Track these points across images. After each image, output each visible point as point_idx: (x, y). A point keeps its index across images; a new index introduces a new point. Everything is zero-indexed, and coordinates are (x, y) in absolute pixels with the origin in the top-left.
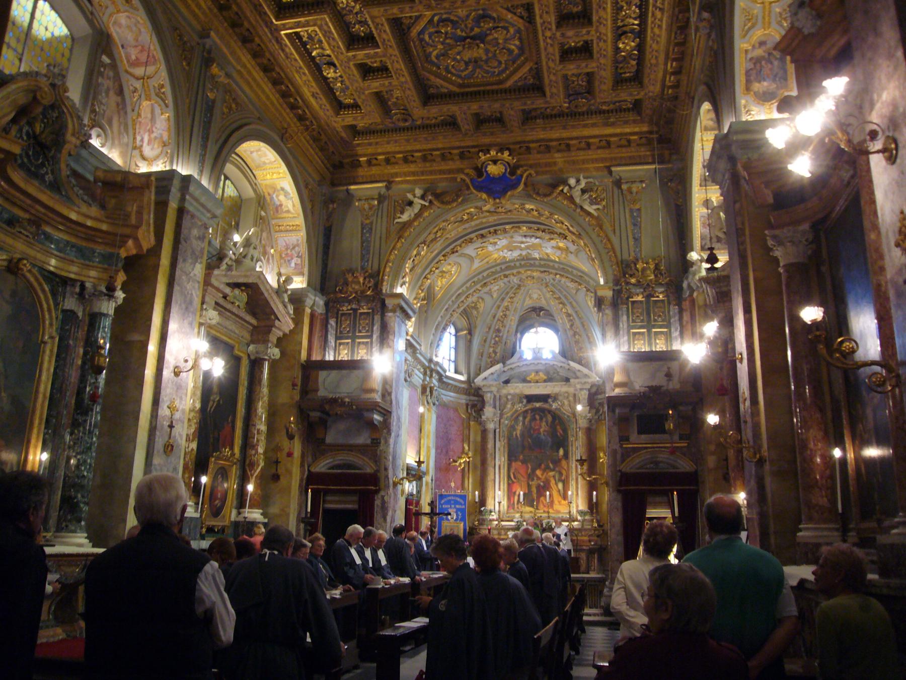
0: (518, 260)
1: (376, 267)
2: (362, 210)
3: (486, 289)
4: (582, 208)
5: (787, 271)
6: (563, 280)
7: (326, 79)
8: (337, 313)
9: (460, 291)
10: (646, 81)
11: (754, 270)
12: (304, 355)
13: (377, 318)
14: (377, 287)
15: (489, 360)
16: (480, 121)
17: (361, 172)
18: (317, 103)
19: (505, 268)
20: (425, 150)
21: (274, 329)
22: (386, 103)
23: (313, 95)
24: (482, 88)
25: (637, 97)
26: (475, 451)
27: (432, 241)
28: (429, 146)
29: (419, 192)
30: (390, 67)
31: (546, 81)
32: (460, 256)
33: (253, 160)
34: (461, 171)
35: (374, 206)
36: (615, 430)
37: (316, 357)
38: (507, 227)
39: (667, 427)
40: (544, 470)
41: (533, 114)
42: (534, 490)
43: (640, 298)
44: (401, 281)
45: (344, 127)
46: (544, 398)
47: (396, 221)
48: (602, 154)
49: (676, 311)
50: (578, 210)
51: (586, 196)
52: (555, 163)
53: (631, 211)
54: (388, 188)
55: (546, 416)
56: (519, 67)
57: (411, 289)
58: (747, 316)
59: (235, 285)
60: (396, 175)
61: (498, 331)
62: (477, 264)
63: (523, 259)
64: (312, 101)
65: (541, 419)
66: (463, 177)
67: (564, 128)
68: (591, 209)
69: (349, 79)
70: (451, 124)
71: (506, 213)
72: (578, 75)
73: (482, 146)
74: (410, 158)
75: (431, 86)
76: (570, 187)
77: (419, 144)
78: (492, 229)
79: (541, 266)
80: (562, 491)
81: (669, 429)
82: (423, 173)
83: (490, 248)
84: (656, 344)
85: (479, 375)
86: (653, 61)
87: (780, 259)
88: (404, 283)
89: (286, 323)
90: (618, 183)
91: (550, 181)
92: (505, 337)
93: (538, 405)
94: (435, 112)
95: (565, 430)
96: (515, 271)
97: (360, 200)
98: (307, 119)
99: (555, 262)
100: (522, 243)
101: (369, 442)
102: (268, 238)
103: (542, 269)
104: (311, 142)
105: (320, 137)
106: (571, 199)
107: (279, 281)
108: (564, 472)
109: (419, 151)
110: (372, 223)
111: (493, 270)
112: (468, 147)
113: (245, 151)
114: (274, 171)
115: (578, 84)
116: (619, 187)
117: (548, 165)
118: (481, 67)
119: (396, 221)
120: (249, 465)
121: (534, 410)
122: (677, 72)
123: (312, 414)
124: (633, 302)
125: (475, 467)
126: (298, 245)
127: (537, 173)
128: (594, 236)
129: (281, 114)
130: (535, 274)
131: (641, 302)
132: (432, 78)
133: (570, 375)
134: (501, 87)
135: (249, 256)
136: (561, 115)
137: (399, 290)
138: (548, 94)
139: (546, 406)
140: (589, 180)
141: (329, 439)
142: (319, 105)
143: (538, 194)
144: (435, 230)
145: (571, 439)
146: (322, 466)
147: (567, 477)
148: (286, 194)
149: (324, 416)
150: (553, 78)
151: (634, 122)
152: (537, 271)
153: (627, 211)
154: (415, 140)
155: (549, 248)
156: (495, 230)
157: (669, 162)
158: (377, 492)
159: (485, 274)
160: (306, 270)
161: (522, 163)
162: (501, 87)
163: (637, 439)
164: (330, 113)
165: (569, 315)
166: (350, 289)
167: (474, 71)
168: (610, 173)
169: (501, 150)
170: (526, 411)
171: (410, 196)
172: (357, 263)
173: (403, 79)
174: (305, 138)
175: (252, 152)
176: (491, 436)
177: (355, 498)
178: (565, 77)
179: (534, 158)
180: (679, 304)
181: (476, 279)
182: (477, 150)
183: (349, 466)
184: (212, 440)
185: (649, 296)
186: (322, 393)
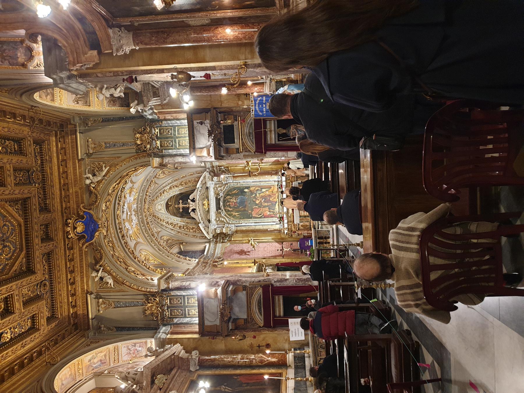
0: (138, 217)
1: (142, 297)
2: (106, 309)
3: (156, 235)
4: (104, 176)
5: (138, 44)
6: (149, 190)
7: (11, 339)
8: (170, 318)
9: (157, 249)
10: (20, 136)
11: (139, 66)
12: (196, 336)
13: (173, 293)
14: (153, 295)
15: (197, 232)
16: (47, 238)
17: (80, 312)
18: (29, 344)
19: (144, 225)
20: (66, 272)
21: (180, 356)
22: (32, 298)
23: (24, 347)
24: (23, 236)
25: (32, 142)
26: (247, 236)
27: (126, 264)
28: (64, 269)
29: (94, 274)
30: (4, 296)
31: (19, 196)
32: (135, 249)
33: (68, 383)
34: (81, 250)
35: (103, 301)
36: (233, 156)
37: (196, 328)
38: (117, 222)
39: (230, 124)
40: (256, 199)
41: (43, 205)
42: (266, 204)
43: (158, 142)
44: (150, 281)
45: (48, 325)
46: (218, 201)
47: (112, 286)
48: (70, 164)
49: (165, 122)
50: (106, 178)
51: (97, 173)
52: (76, 192)
53: (106, 147)
54: (91, 293)
55: (227, 199)
56: (8, 212)
57: (155, 275)
58: (165, 71)
59: (153, 382)
60: (83, 289)
61: (180, 227)
62: (141, 240)
63: (138, 213)
64: (27, 348)
65: (229, 202)
66: (84, 247)
67: (52, 186)
68: (105, 171)
69: (12, 323)
70: (49, 256)
71: (108, 221)
72: (16, 177)
73: (64, 236)
74: (71, 281)
75: (21, 269)
76: (91, 183)
77: (62, 276)
78: (119, 231)
79: (141, 203)
80: (267, 189)
81: (231, 122)
82: (82, 272)
83: (131, 232)
84: (185, 133)
85: (206, 237)
86: (6, 130)
87: (131, 48)
88: (152, 280)
89: (177, 348)
90: (89, 155)
91: (88, 194)
92: (184, 224)
93: (221, 204)
94: (40, 266)
95: (234, 189)
96: (145, 218)
97: (99, 310)
98: (41, 350)
99: (139, 195)
100: (127, 214)
101: (245, 292)
102: (122, 367)
103: (144, 203)
104: (57, 345)
105: (55, 339)
106: (99, 182)
107: (149, 356)
108: (257, 188)
109: (67, 275)
110: (114, 302)
111: (144, 231)
112: (65, 245)
113: (61, 389)
114: (76, 368)
115: (22, 177)
116: (92, 154)
117: (77, 196)
118: (8, 238)
119: (112, 286)
120: (262, 363)
121: (224, 206)
122: (14, 115)
123: (230, 328)
124: (161, 146)
125: (256, 236)
126: (128, 347)
127: (83, 203)
128: (121, 169)
129: (36, 367)
130: (146, 207)
131: (161, 142)
132: (14, 268)
133: (204, 187)
134: (23, 225)
135: (134, 376)
136: (44, 189)
137: (156, 282)
138: (29, 195)
139: (222, 199)
140: (87, 171)
141: (245, 317)
142: (30, 343)
143: (96, 202)
144: (118, 262)
145: (239, 185)
146: (260, 319)
147: (259, 187)
148: (94, 358)
149: (231, 320)
150: (17, 192)
151: (49, 145)
152: (144, 206)
153: (106, 150)
154: (59, 278)
155: (130, 199)
156: (119, 229)
157: (75, 125)
158: (272, 285)
159: (146, 235)
160: (143, 340)
161: (75, 212)
162: (23, 225)
163: (237, 144)
164: (37, 334)
165: (171, 188)
166: (155, 311)
167: (10, 242)
168: (82, 159)
169: (67, 225)
170: (225, 210)
171: (97, 279)
172: (140, 309)
173: (14, 287)
174: (54, 350)
175: (63, 384)
176: (239, 228)
177: (277, 297)
178: (16, 185)
179: (73, 204)
180: (162, 121)
181: (150, 241)
182: (67, 239)
183: (259, 302)
184: (248, 387)
185: (158, 138)
186: (218, 322)
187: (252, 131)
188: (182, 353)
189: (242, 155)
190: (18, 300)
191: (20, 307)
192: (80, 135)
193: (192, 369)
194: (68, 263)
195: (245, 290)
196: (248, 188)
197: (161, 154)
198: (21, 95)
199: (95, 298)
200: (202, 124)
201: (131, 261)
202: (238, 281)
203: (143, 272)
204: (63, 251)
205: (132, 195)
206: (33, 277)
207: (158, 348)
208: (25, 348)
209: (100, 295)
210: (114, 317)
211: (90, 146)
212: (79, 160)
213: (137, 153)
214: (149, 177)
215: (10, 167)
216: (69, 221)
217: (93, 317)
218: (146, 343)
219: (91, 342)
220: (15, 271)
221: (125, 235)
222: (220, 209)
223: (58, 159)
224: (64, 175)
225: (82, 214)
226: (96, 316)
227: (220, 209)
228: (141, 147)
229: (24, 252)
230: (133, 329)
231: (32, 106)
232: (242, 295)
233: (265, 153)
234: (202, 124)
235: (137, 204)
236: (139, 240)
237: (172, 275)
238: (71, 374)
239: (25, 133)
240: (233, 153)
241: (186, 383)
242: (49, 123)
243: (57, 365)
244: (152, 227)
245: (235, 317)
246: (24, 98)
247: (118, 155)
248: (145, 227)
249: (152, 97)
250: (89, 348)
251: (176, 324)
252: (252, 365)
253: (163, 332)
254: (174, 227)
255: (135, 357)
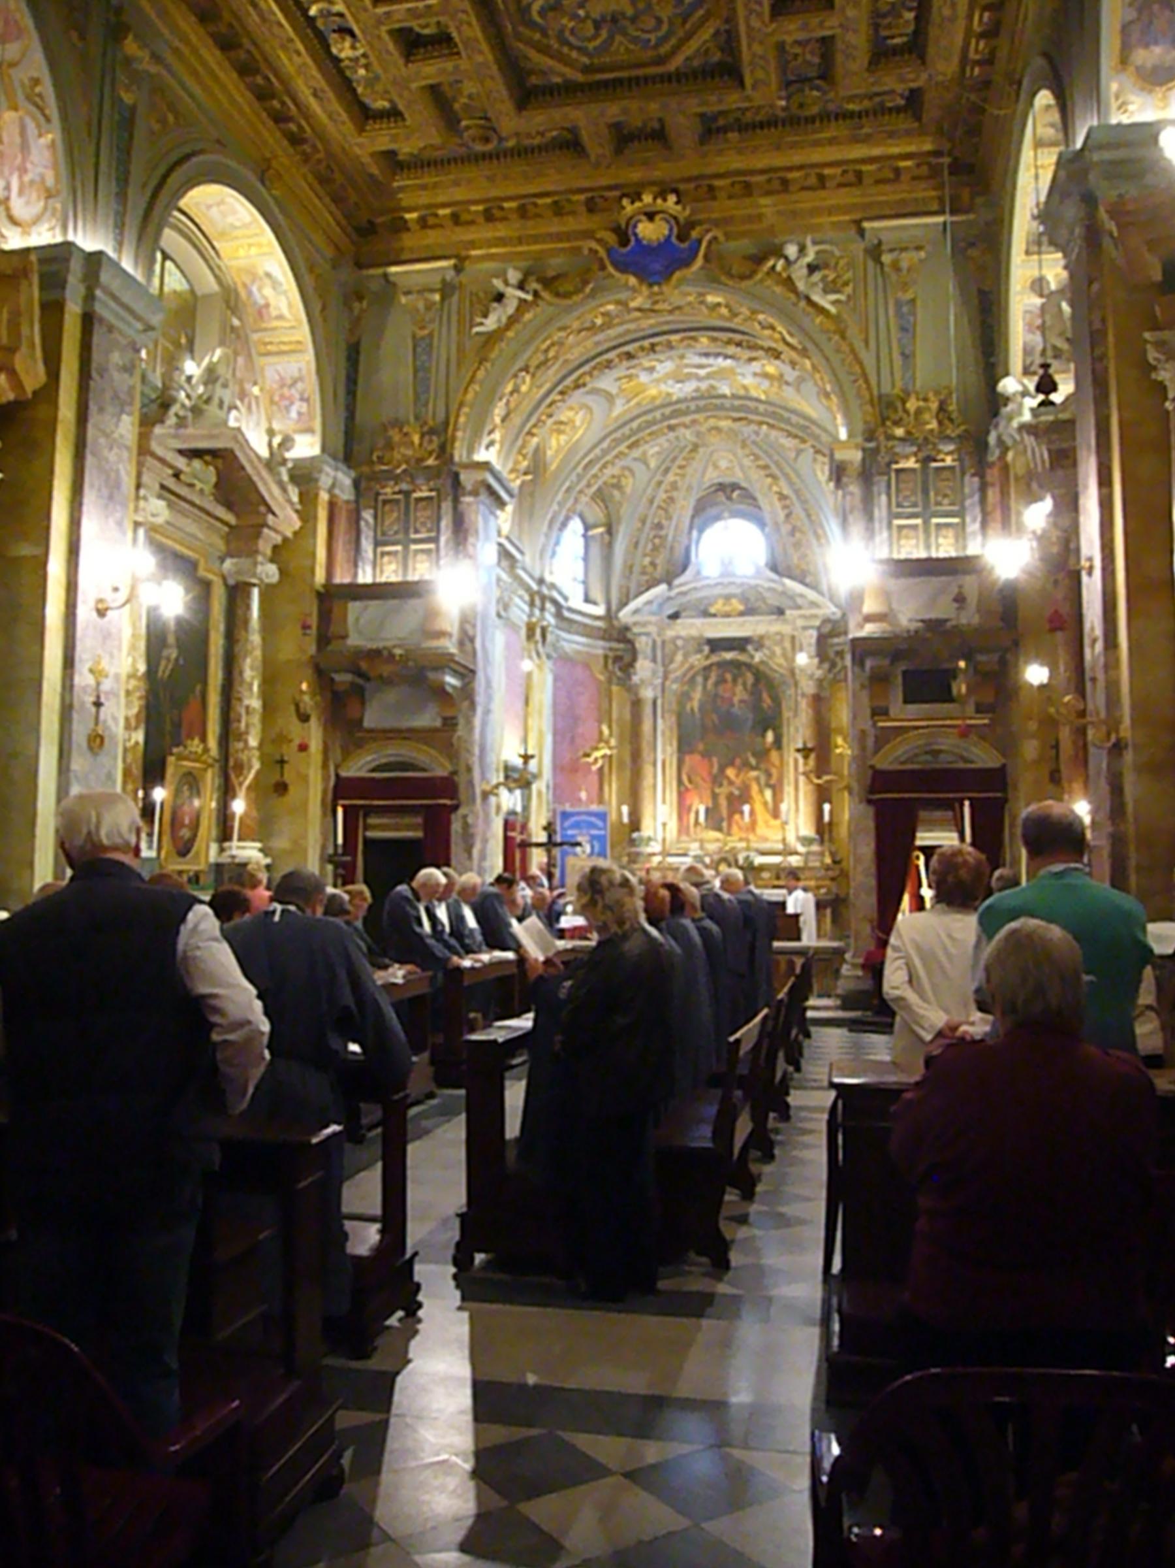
0: (693, 399)
1: (441, 416)
3: (636, 453)
7: (336, 60)
8: (376, 500)
10: (931, 51)
11: (1120, 409)
12: (320, 577)
13: (447, 506)
14: (444, 452)
16: (624, 138)
17: (408, 241)
19: (672, 413)
21: (266, 530)
23: (315, 95)
25: (913, 85)
27: (538, 367)
29: (514, 276)
30: (455, 34)
32: (588, 393)
34: (588, 234)
35: (434, 303)
36: (864, 696)
37: (341, 577)
39: (955, 691)
40: (739, 770)
41: (721, 122)
43: (911, 463)
44: (486, 440)
45: (373, 155)
46: (739, 644)
50: (803, 304)
51: (817, 277)
52: (760, 217)
53: (899, 304)
54: (458, 269)
55: (742, 675)
57: (505, 455)
58: (1105, 491)
59: (194, 454)
61: (659, 526)
62: (619, 408)
65: (735, 680)
66: (594, 245)
68: (825, 301)
75: (531, 72)
77: (512, 185)
78: (646, 343)
79: (734, 409)
82: (520, 241)
83: (644, 378)
84: (938, 546)
85: (626, 604)
88: (491, 444)
89: (286, 520)
90: (875, 252)
91: (753, 250)
92: (670, 538)
93: (729, 656)
94: (542, 122)
96: (687, 419)
101: (438, 723)
105: (332, 177)
106: (789, 283)
108: (774, 771)
110: (431, 335)
113: (197, 204)
117: (750, 219)
123: (338, 677)
131: (913, 470)
133: (783, 602)
135: (216, 401)
136: (771, 123)
137: (481, 456)
139: (743, 658)
142: (324, 111)
145: (786, 714)
146: (359, 767)
148: (275, 284)
149: (360, 681)
151: (908, 133)
152: (727, 418)
154: (506, 177)
155: (748, 377)
158: (456, 808)
159: (635, 425)
160: (317, 424)
162: (659, 70)
163: (902, 713)
164: (349, 127)
165: (782, 497)
167: (611, 37)
168: (861, 232)
169: (662, 195)
171: (498, 284)
172: (405, 407)
173: (480, 59)
175: (209, 207)
176: (648, 710)
179: (722, 207)
180: (980, 474)
182: (617, 193)
187: (944, 762)
188: (272, 534)
189: (867, 725)
190: (443, 71)
191: (425, 78)
192: (936, 224)
193: (228, 564)
194: (548, 200)
195: (444, 724)
196: (778, 743)
197: (874, 471)
198: (1046, 55)
199: (444, 281)
200: (956, 600)
201: (555, 379)
202: (473, 706)
203: (517, 420)
204: (586, 184)
205: (758, 380)
206: (508, 106)
207: (290, 465)
208: (312, 100)
209: (452, 295)
210: (390, 334)
211: (904, 255)
212: (858, 223)
213: (880, 397)
214: (817, 431)
215: (832, 28)
216: (672, 198)
217: (392, 279)
218: (310, 430)
219: (318, 276)
220: (526, 58)
221: (635, 362)
222: (712, 651)
223: (864, 161)
224: (813, 180)
225: (694, 234)
226: (394, 285)
227: (712, 651)
228: (896, 410)
229: (580, 78)
230: (351, 392)
231: (1020, 83)
232: (428, 718)
233: (869, 802)
234: (956, 600)
235: (734, 397)
236: (619, 402)
237: (502, 504)
238: (236, 228)
239: (941, 66)
240: (872, 697)
241: (188, 548)
242: (974, 131)
243: (263, 190)
244: (662, 440)
245: (367, 694)
246: (1039, 62)
247: (872, 343)
248: (661, 421)
249: (1054, 447)
250: (303, 270)
251: (358, 518)
252: (231, 738)
253: (337, 481)
254: (659, 507)
255: (272, 402)
